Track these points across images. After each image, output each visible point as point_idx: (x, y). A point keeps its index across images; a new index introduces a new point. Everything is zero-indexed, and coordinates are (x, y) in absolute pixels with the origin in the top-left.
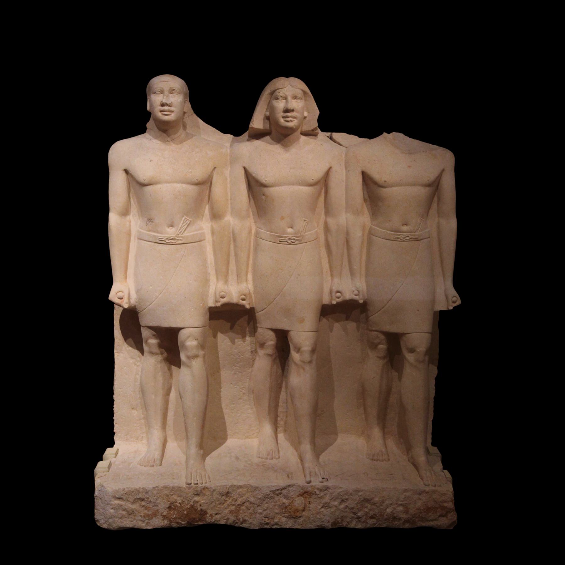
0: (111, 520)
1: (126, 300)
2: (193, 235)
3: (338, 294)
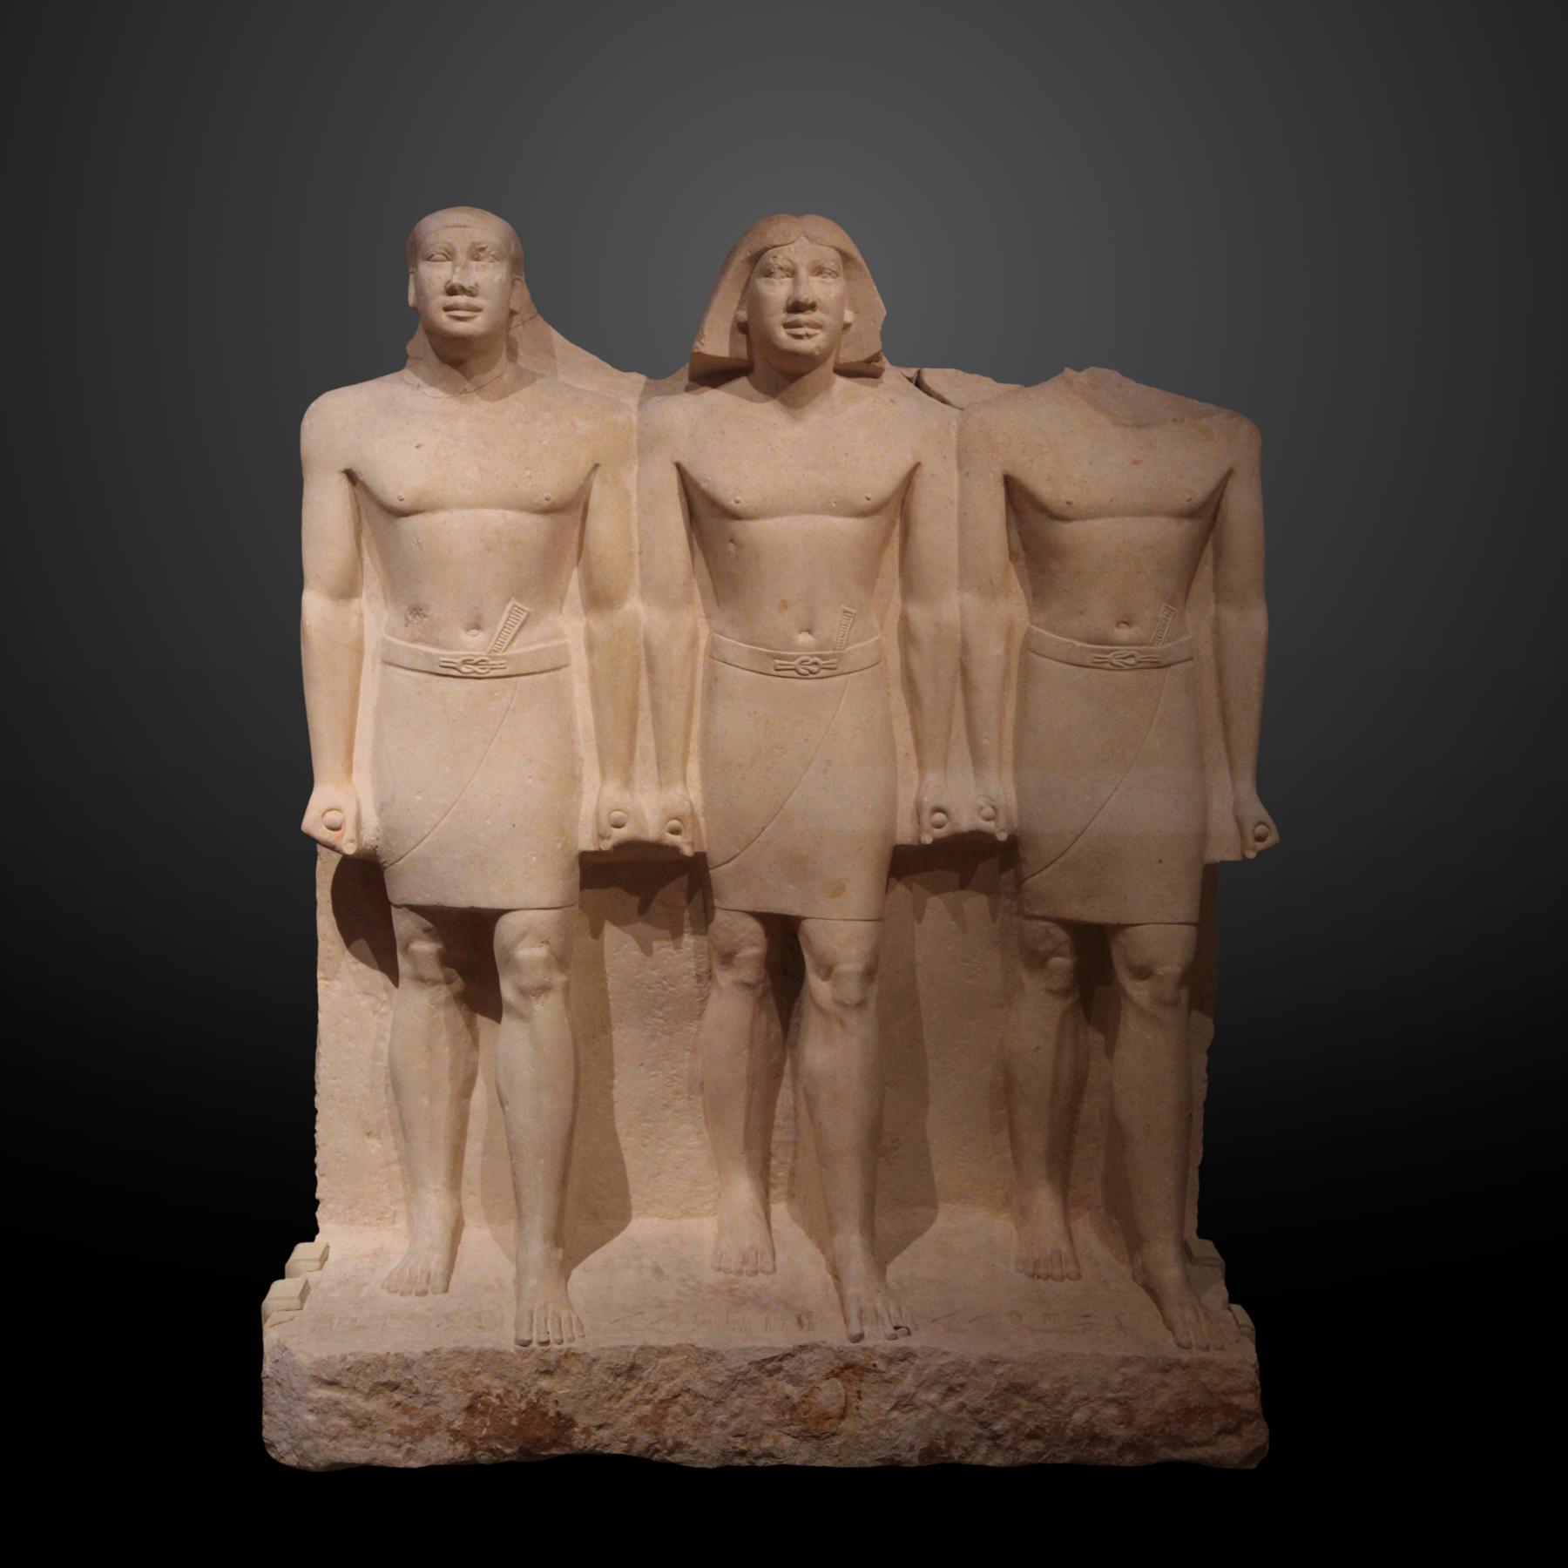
0: (307, 1444)
1: (349, 832)
2: (536, 652)
3: (939, 817)
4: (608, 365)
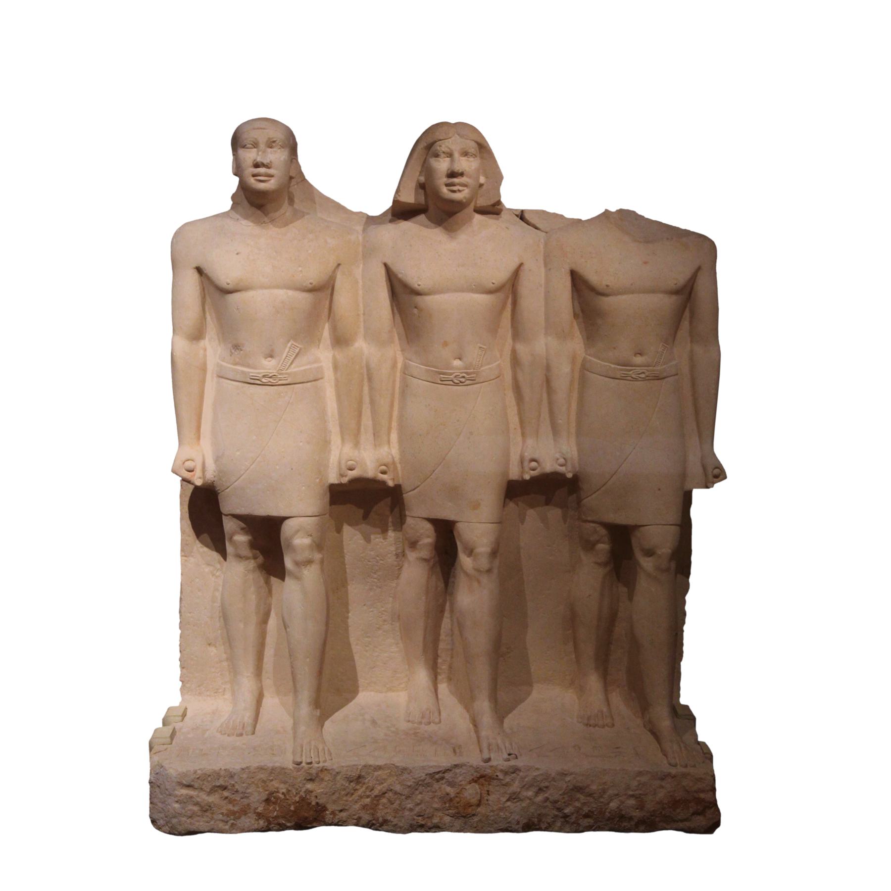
1: (198, 473)
2: (305, 370)
3: (534, 464)
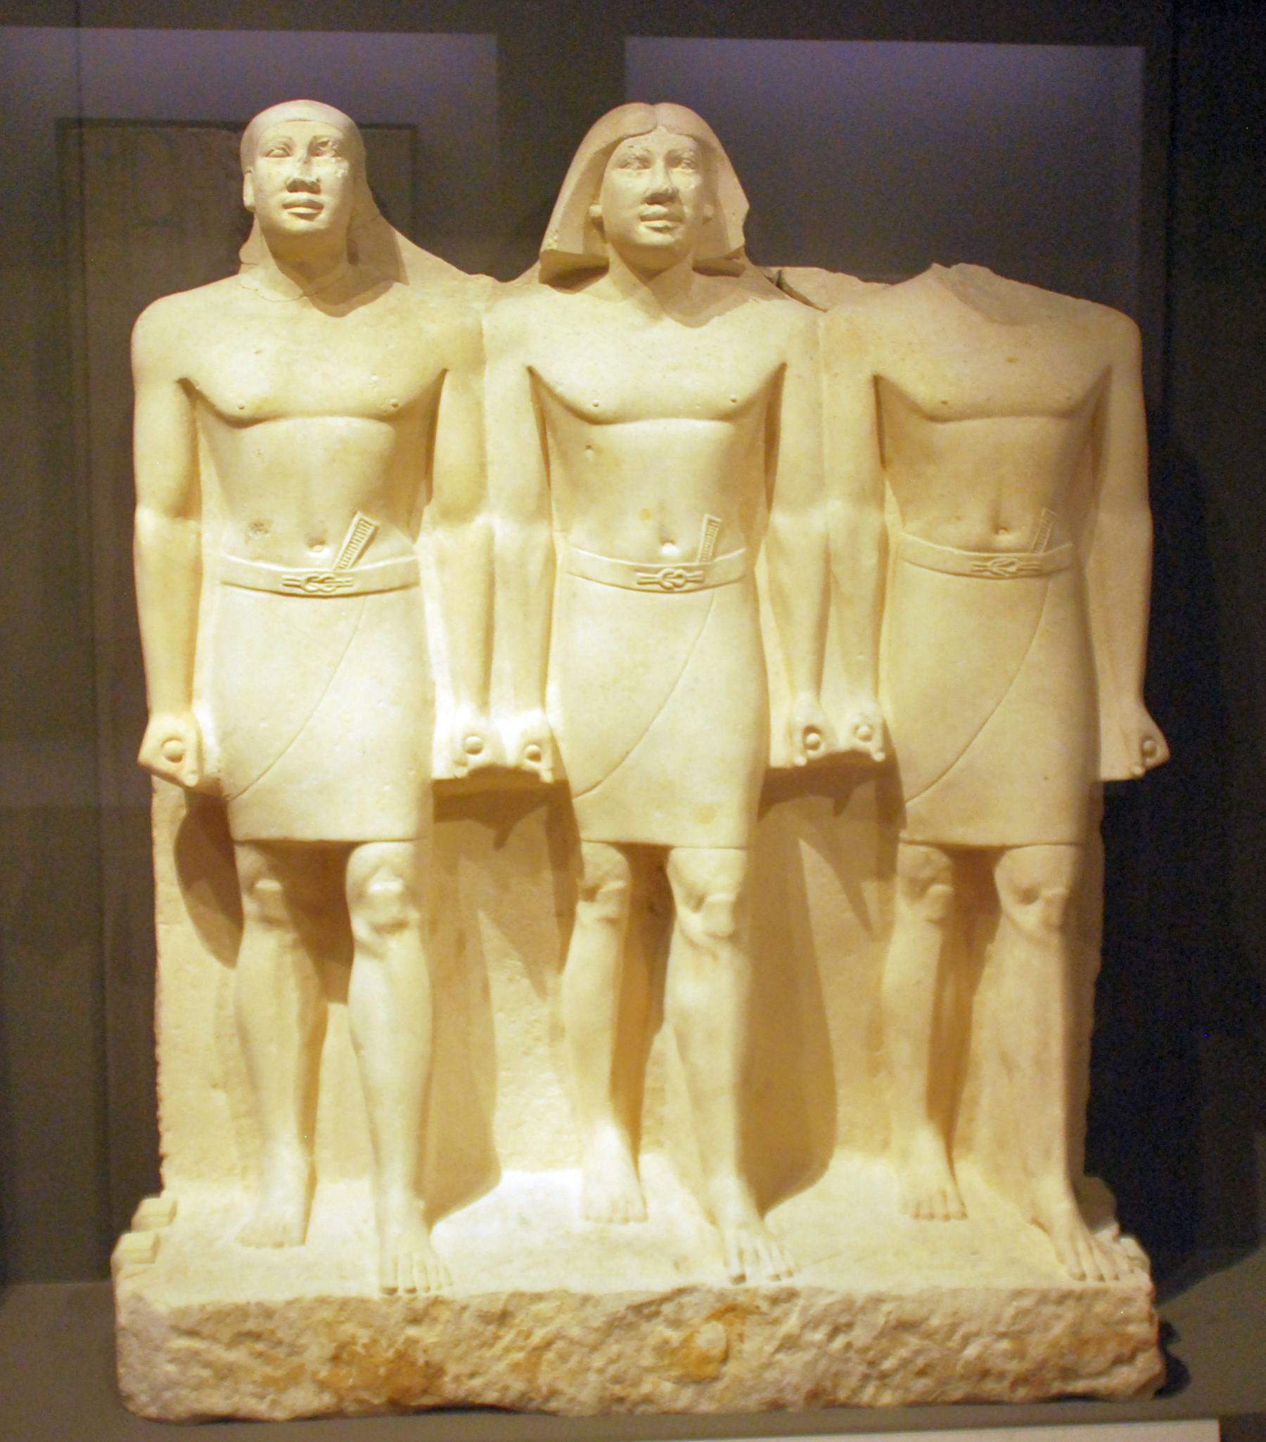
0: (168, 1395)
1: (189, 763)
2: (384, 569)
3: (813, 737)
4: (454, 269)
